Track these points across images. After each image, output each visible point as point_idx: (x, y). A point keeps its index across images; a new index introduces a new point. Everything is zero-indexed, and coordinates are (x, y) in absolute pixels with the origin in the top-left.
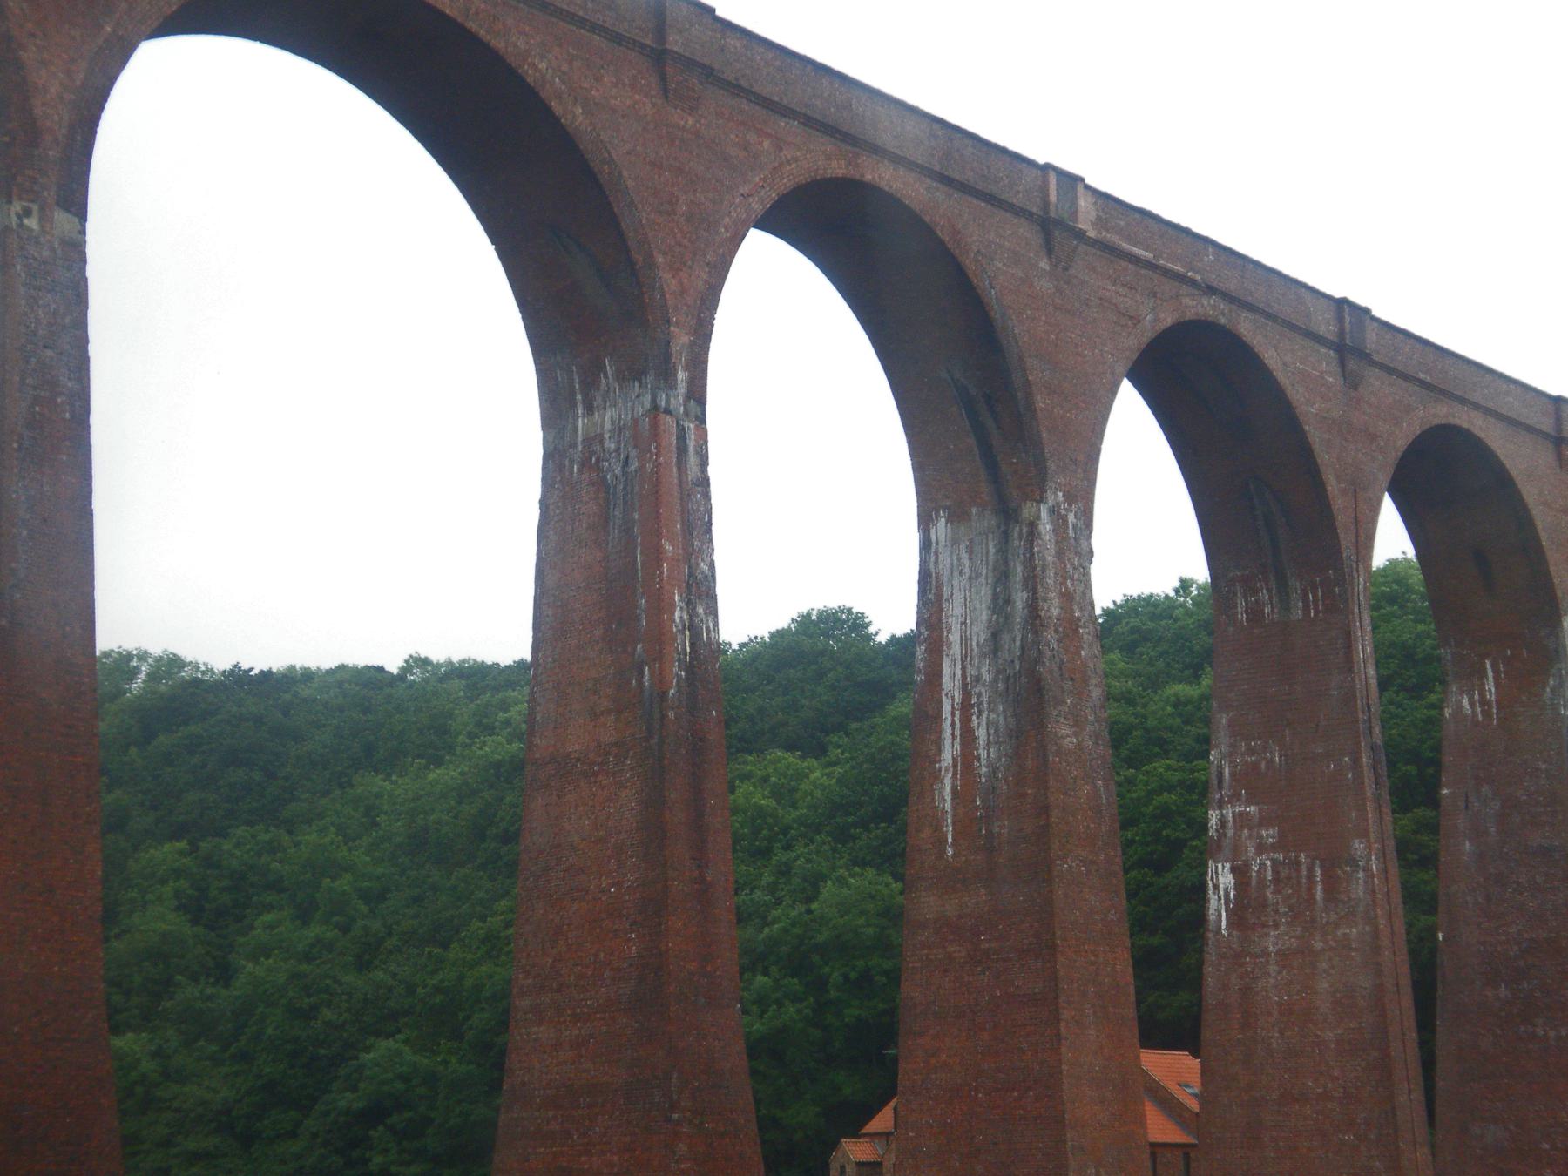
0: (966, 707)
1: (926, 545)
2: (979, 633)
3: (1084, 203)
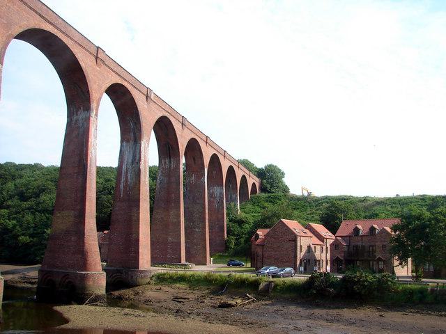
0: (127, 173)
1: (121, 146)
2: (130, 160)
3: (152, 94)
